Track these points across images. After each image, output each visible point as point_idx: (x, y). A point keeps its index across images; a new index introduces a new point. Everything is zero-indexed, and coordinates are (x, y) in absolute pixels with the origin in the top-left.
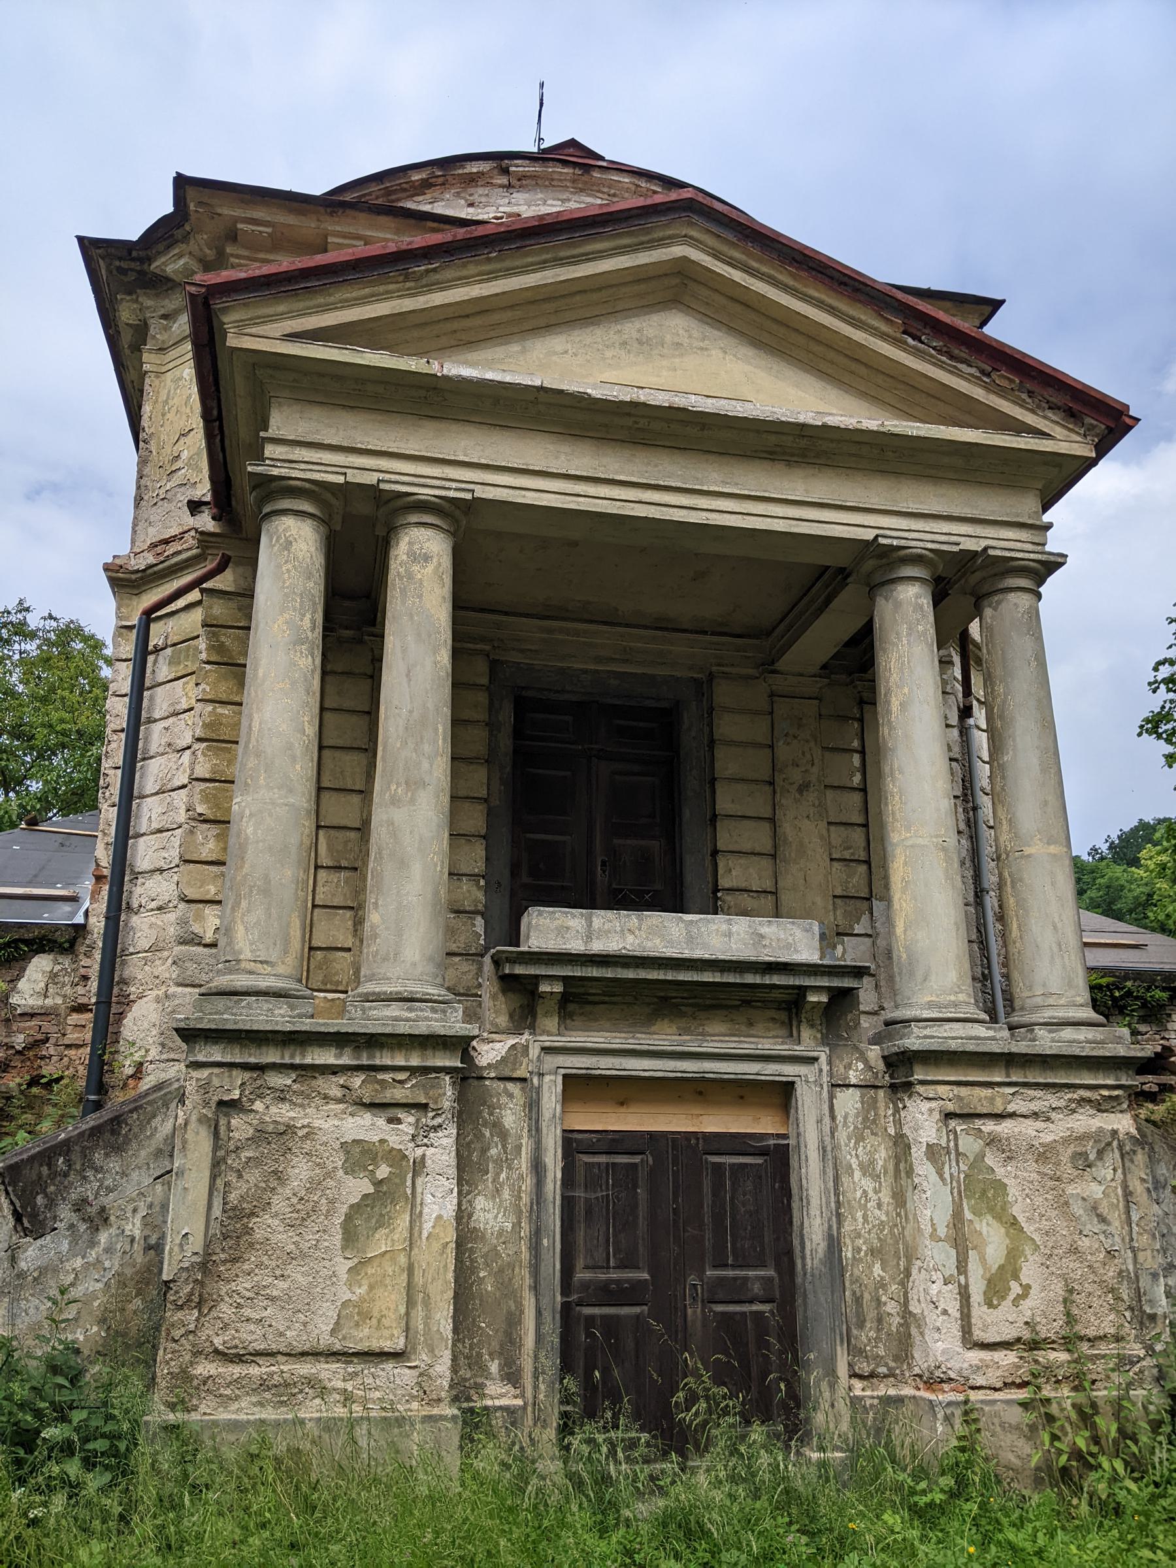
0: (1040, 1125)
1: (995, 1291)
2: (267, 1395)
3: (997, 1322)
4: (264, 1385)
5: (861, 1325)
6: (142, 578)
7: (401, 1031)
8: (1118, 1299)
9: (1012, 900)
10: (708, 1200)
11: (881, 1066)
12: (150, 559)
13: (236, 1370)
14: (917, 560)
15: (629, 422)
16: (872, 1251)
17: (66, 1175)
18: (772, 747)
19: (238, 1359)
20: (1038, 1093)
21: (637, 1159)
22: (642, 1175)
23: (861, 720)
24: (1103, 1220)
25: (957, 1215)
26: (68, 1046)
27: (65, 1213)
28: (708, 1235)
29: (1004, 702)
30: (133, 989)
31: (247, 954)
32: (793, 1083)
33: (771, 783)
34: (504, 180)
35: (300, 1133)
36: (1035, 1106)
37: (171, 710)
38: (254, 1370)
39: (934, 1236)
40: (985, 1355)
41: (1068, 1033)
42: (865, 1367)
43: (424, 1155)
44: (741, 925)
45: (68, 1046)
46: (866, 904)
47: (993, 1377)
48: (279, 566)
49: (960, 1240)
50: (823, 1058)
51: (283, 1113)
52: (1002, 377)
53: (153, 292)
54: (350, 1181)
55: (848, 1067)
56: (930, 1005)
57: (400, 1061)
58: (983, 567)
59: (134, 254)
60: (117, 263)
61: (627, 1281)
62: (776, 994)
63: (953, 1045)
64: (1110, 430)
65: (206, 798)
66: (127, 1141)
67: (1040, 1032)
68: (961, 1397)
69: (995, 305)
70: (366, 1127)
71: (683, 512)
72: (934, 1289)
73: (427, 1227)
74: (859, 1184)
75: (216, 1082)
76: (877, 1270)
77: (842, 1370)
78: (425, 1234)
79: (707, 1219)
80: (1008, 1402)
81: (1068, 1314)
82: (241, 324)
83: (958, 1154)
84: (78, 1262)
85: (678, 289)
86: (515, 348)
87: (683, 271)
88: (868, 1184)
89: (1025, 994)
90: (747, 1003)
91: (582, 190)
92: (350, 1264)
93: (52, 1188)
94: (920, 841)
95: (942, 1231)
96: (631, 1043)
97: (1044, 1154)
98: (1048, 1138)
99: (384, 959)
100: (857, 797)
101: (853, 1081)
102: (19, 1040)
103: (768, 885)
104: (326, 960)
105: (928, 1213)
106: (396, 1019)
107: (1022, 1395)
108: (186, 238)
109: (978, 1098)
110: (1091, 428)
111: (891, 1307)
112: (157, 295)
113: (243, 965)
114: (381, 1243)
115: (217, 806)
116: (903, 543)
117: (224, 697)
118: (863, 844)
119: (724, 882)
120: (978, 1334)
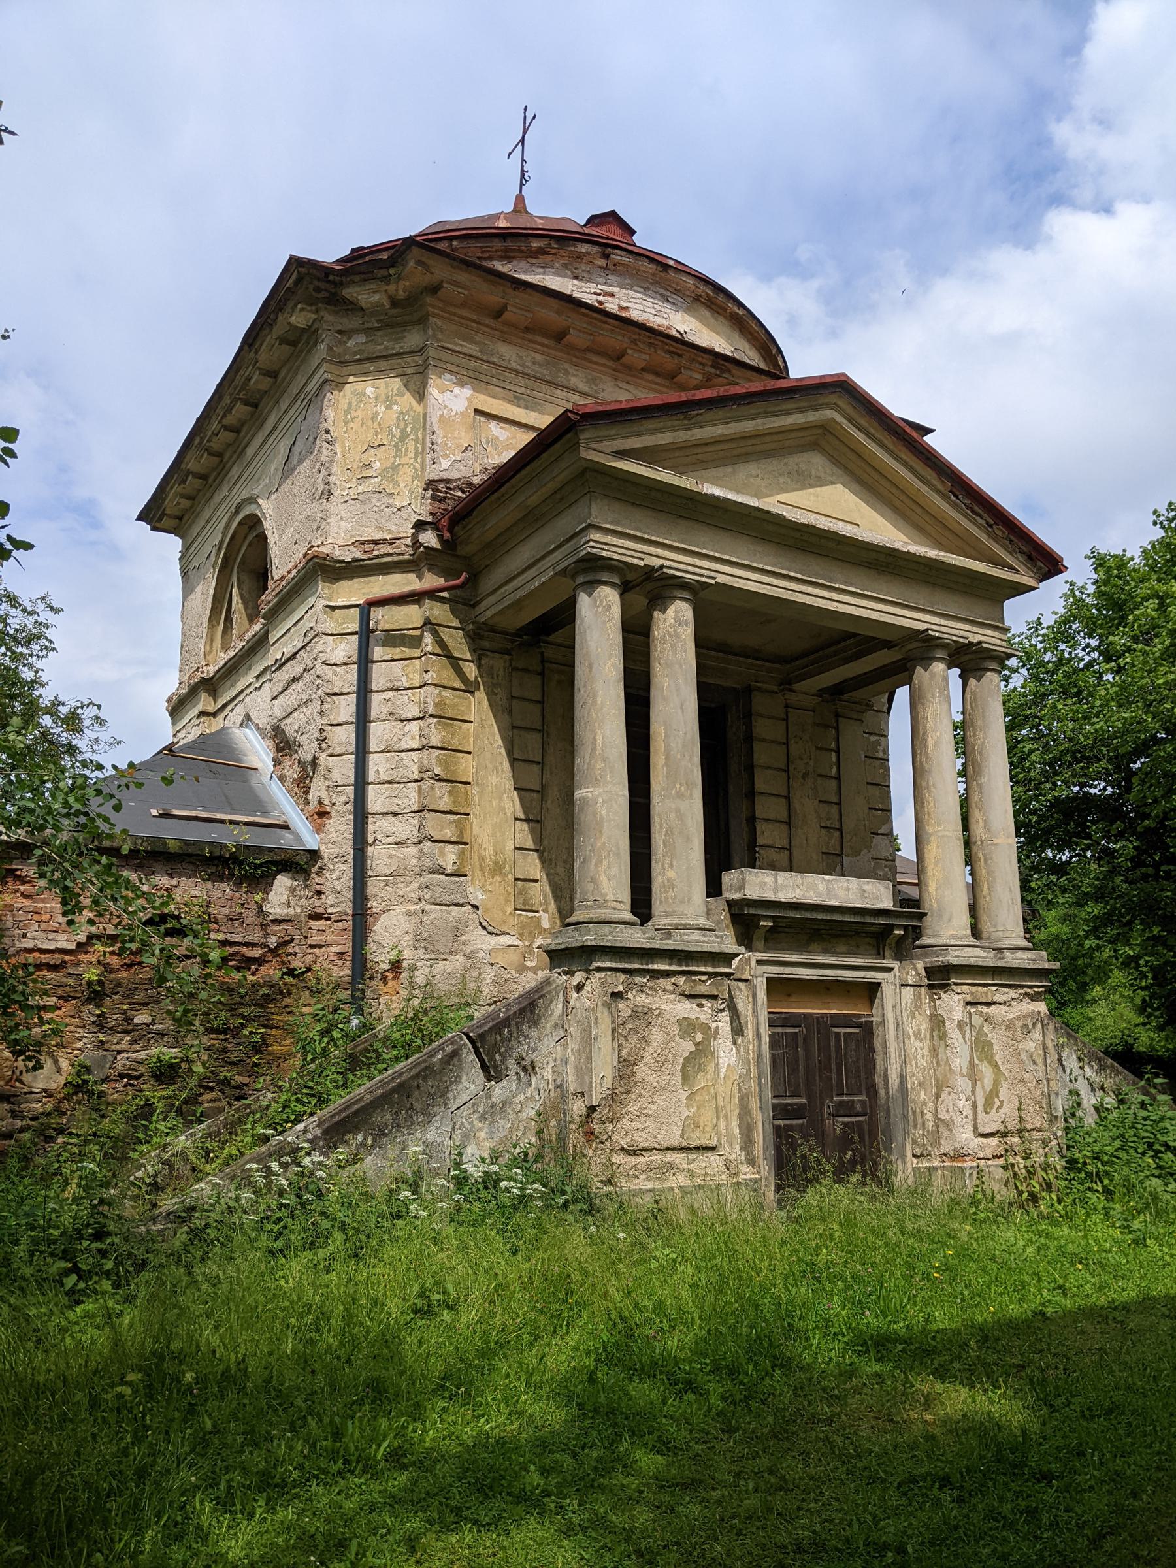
0: (1007, 1008)
1: (988, 1104)
2: (650, 1174)
3: (990, 1123)
4: (650, 1168)
5: (915, 1127)
6: (344, 568)
7: (705, 950)
8: (1041, 1107)
9: (984, 871)
10: (833, 1055)
11: (923, 973)
12: (358, 554)
13: (633, 1160)
14: (945, 646)
15: (798, 535)
16: (920, 1084)
17: (510, 1041)
18: (787, 744)
19: (634, 1153)
20: (1006, 990)
21: (797, 1030)
22: (801, 1039)
23: (837, 729)
24: (1035, 1063)
25: (971, 1063)
26: (312, 946)
27: (513, 1067)
28: (834, 1076)
29: (983, 743)
30: (375, 904)
31: (610, 897)
32: (879, 984)
33: (787, 771)
34: (603, 263)
35: (656, 1013)
36: (1005, 998)
37: (390, 685)
38: (640, 1159)
39: (961, 1074)
40: (984, 1140)
41: (1019, 954)
42: (918, 1152)
43: (717, 1027)
44: (854, 883)
45: (312, 946)
46: (838, 859)
47: (988, 1153)
48: (605, 623)
49: (974, 1077)
50: (897, 968)
51: (643, 1000)
52: (999, 530)
53: (332, 308)
54: (683, 1043)
55: (907, 974)
56: (953, 937)
57: (702, 969)
58: (975, 652)
59: (331, 277)
60: (316, 283)
61: (796, 1104)
62: (873, 929)
63: (972, 962)
64: (1049, 571)
65: (440, 762)
66: (539, 1018)
67: (1007, 953)
68: (975, 1164)
69: (929, 431)
70: (687, 1008)
71: (824, 601)
72: (961, 1104)
73: (723, 1071)
74: (914, 1044)
75: (609, 980)
76: (922, 1095)
77: (909, 1153)
78: (722, 1076)
79: (833, 1066)
80: (996, 1166)
81: (1020, 1117)
82: (590, 440)
83: (971, 1026)
84: (522, 1097)
85: (821, 440)
86: (729, 469)
87: (826, 429)
88: (917, 1044)
89: (991, 930)
90: (857, 933)
91: (657, 282)
92: (687, 1094)
93: (503, 1049)
94: (947, 833)
95: (965, 1071)
96: (795, 958)
97: (1009, 1026)
98: (1011, 1016)
99: (682, 902)
100: (834, 783)
101: (910, 982)
102: (273, 940)
103: (785, 843)
104: (524, 889)
105: (958, 1060)
106: (698, 941)
107: (1001, 1161)
108: (386, 279)
109: (981, 993)
110: (1040, 568)
111: (929, 1116)
112: (336, 313)
113: (609, 903)
114: (701, 1082)
115: (447, 769)
116: (941, 635)
117: (445, 683)
118: (837, 817)
119: (760, 841)
120: (982, 1129)
